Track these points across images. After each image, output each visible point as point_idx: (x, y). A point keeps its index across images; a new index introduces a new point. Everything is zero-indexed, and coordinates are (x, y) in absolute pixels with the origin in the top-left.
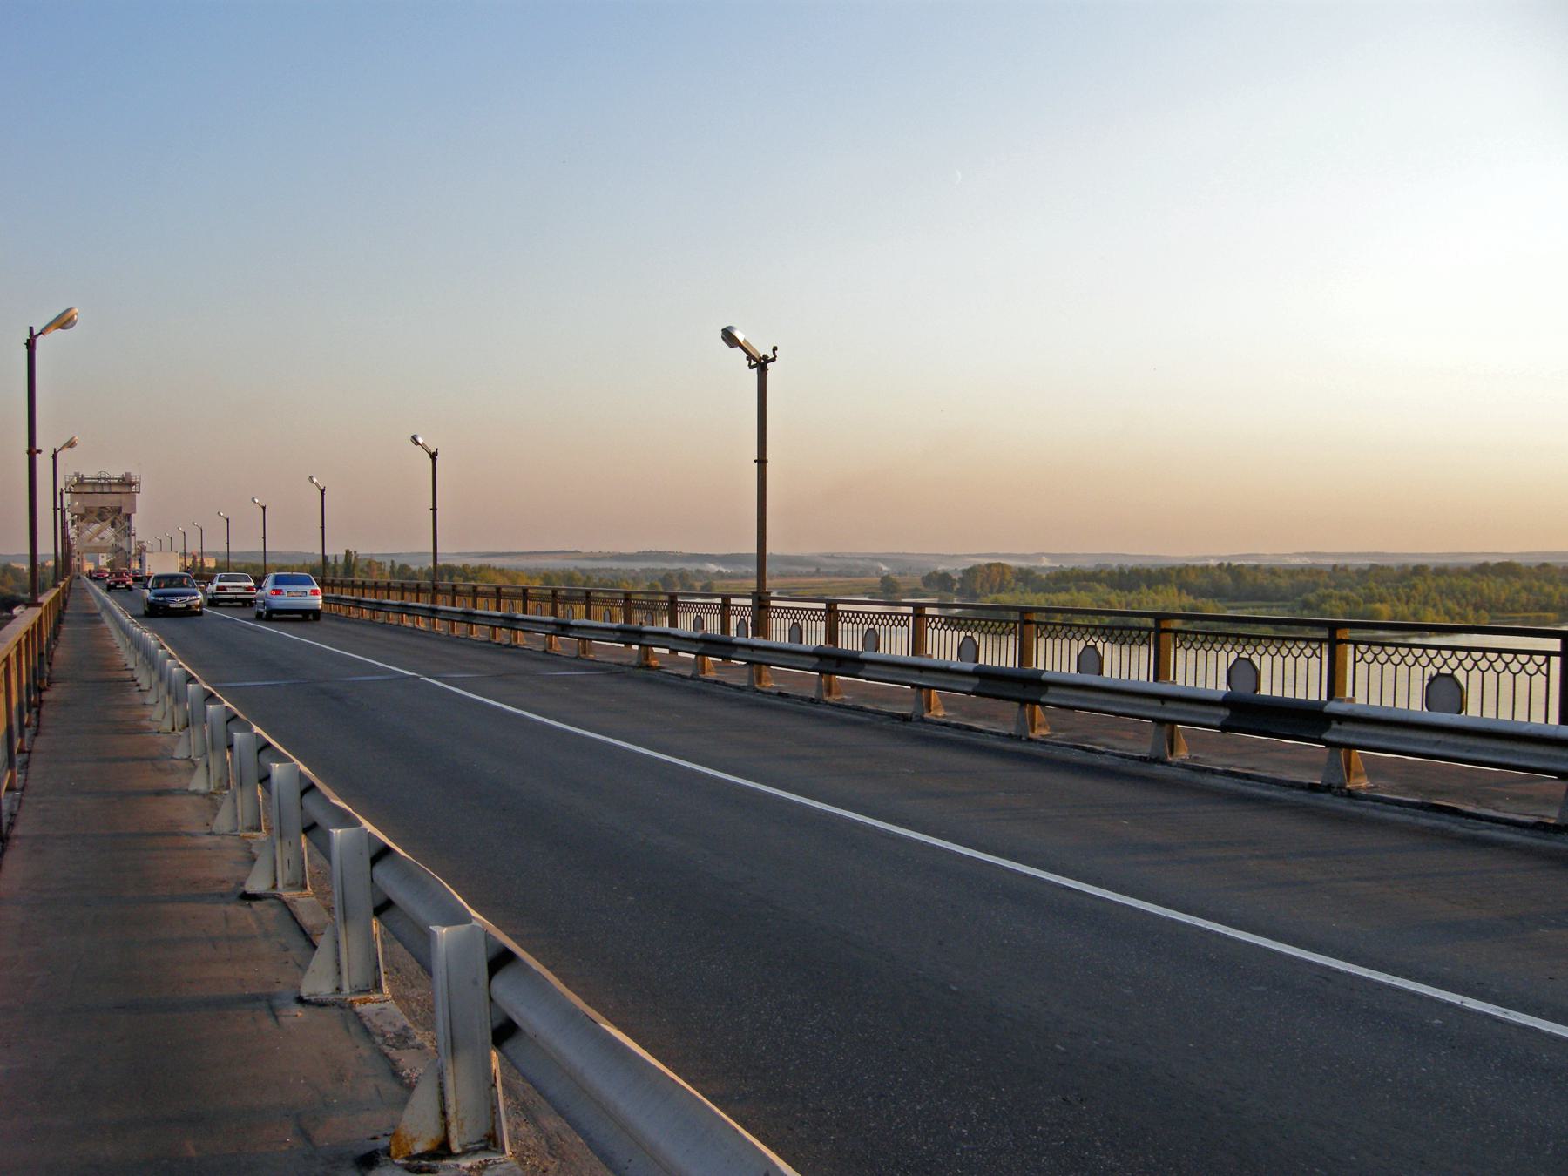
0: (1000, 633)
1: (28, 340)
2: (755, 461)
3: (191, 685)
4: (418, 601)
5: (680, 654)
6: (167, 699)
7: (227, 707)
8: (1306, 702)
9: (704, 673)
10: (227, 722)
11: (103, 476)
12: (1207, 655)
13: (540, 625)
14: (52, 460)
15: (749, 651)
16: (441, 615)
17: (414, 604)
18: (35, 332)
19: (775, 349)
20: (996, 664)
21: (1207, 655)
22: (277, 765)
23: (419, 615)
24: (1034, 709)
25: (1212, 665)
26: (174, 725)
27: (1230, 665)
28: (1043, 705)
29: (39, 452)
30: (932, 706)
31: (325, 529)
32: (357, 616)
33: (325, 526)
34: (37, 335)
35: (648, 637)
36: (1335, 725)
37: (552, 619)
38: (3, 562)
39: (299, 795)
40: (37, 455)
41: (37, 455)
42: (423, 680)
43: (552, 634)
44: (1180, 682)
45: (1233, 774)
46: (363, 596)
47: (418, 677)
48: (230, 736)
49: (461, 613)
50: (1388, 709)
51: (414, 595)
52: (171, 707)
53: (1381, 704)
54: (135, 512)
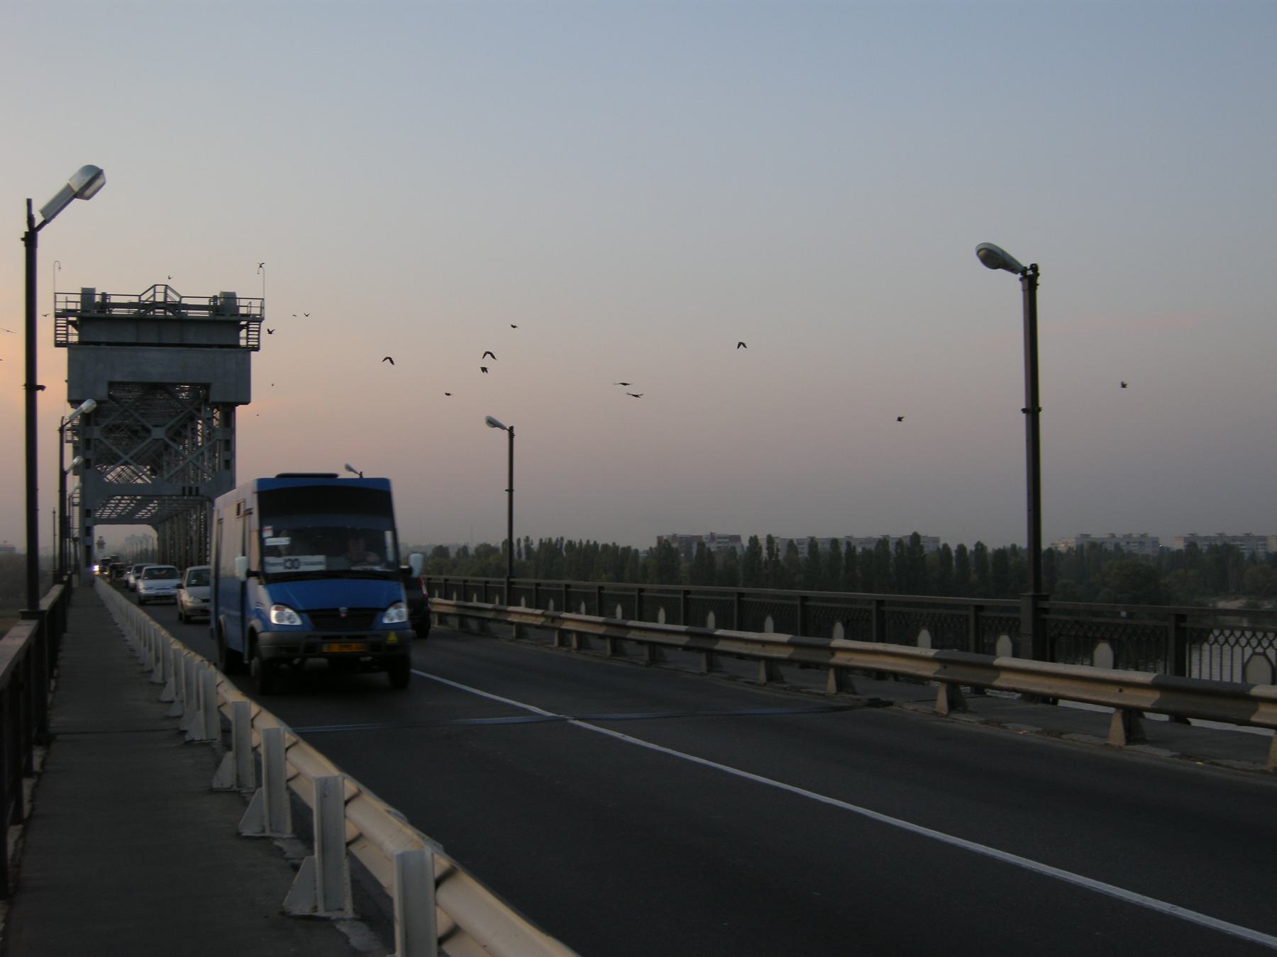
0: (1243, 644)
2: (506, 490)
5: (1195, 722)
8: (1232, 683)
11: (160, 298)
12: (1232, 652)
13: (1104, 688)
14: (21, 249)
15: (1115, 690)
19: (492, 423)
20: (1216, 678)
21: (1232, 652)
25: (1227, 662)
27: (1245, 660)
29: (42, 388)
31: (1043, 417)
33: (515, 487)
35: (513, 615)
42: (573, 725)
44: (1195, 675)
45: (1246, 770)
47: (566, 720)
50: (1216, 682)
53: (1211, 678)
54: (246, 402)
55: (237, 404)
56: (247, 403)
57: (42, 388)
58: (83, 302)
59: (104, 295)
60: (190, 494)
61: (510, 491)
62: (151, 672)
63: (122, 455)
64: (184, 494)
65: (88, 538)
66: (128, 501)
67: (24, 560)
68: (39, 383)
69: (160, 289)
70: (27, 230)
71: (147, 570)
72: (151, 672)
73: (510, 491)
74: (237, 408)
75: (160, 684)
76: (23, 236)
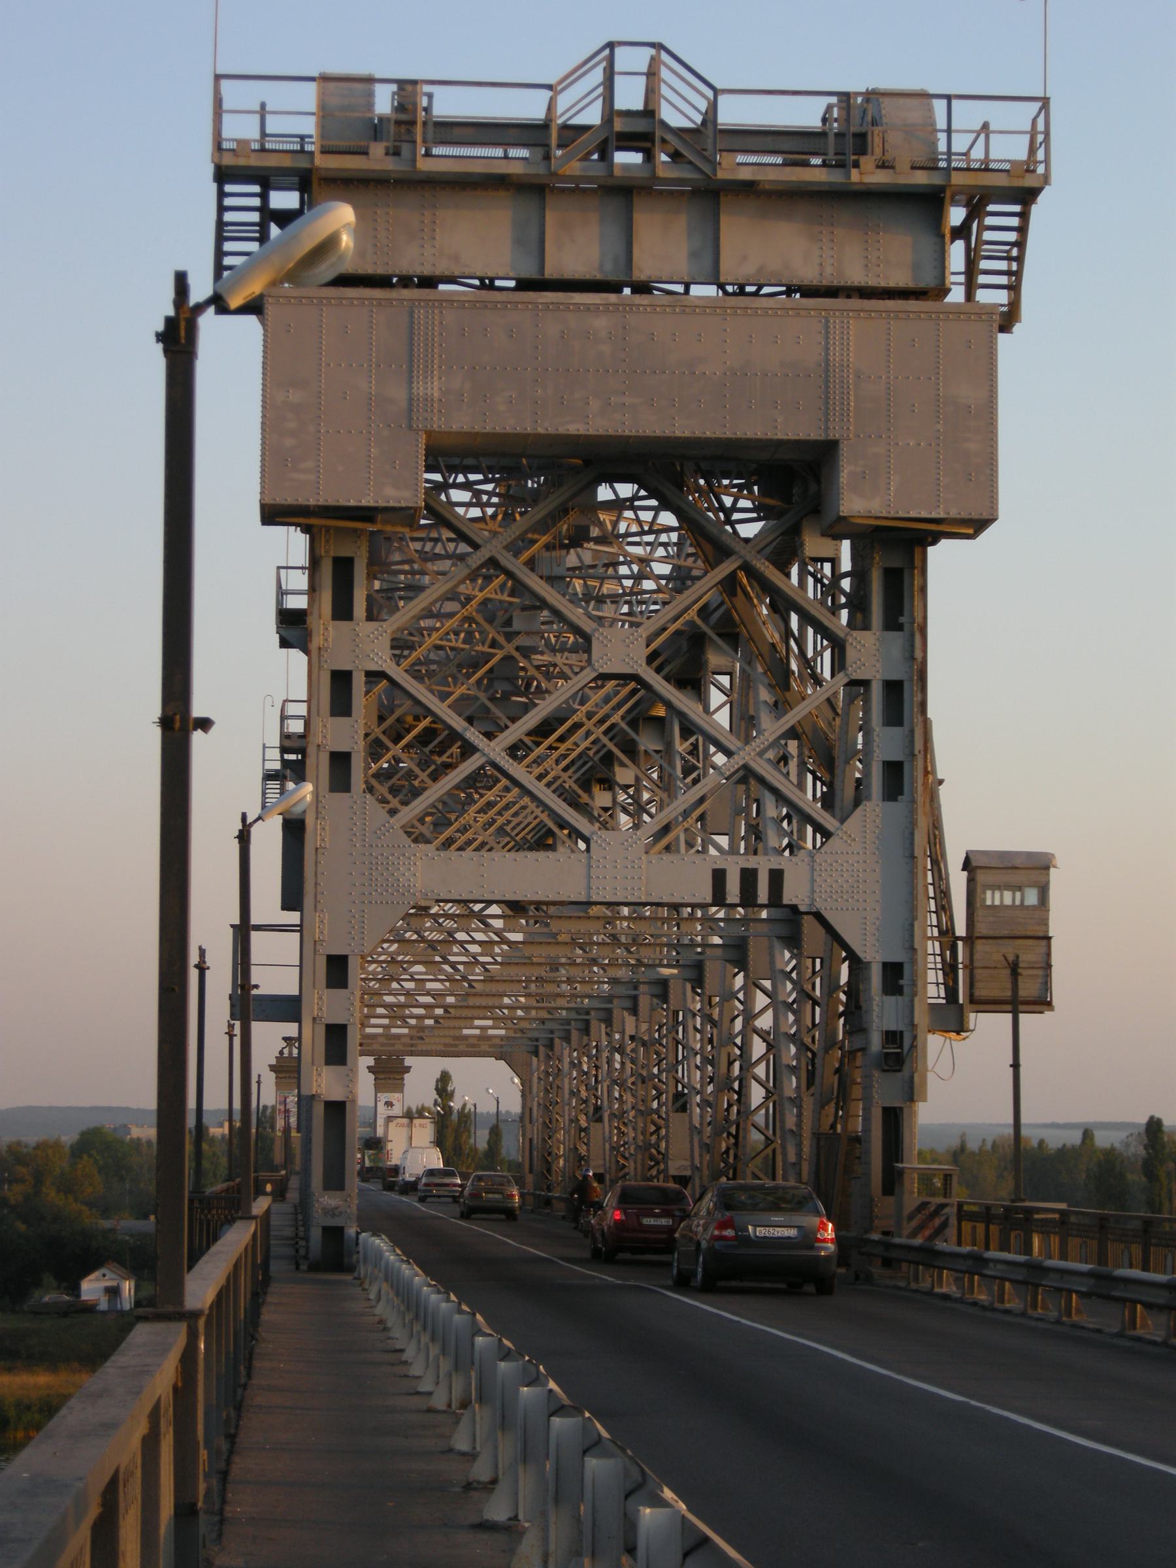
1: (169, 321)
3: (557, 1420)
4: (1064, 1256)
6: (552, 1518)
7: (551, 1391)
9: (1135, 1329)
10: (627, 1497)
16: (1052, 1281)
17: (1136, 1273)
18: (249, 820)
22: (648, 1511)
23: (1004, 1279)
24: (1135, 1308)
26: (451, 1399)
28: (981, 1275)
29: (205, 724)
30: (1006, 1297)
31: (1022, 1070)
32: (1053, 1314)
33: (1022, 1061)
34: (200, 308)
36: (991, 1265)
37: (1022, 1258)
38: (8, 1138)
39: (680, 1556)
40: (197, 736)
41: (197, 736)
43: (917, 1264)
46: (959, 1244)
48: (630, 1524)
49: (1090, 1274)
51: (1136, 1250)
52: (437, 1359)
55: (935, 539)
56: (975, 526)
57: (205, 724)
58: (325, 114)
59: (406, 88)
60: (748, 897)
61: (1016, 1066)
62: (402, 1351)
63: (473, 735)
64: (719, 898)
65: (894, 676)
66: (386, 1021)
67: (1012, 1137)
68: (197, 711)
69: (631, 60)
70: (171, 312)
71: (476, 1176)
72: (402, 1351)
73: (1016, 1066)
74: (931, 550)
75: (464, 1454)
76: (160, 327)
